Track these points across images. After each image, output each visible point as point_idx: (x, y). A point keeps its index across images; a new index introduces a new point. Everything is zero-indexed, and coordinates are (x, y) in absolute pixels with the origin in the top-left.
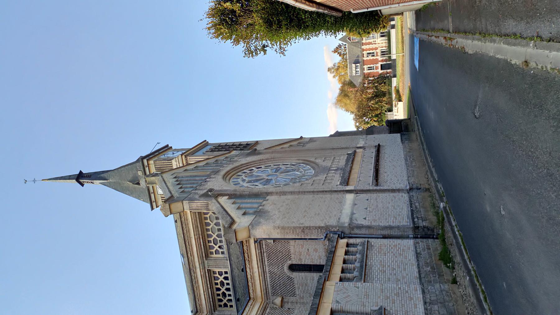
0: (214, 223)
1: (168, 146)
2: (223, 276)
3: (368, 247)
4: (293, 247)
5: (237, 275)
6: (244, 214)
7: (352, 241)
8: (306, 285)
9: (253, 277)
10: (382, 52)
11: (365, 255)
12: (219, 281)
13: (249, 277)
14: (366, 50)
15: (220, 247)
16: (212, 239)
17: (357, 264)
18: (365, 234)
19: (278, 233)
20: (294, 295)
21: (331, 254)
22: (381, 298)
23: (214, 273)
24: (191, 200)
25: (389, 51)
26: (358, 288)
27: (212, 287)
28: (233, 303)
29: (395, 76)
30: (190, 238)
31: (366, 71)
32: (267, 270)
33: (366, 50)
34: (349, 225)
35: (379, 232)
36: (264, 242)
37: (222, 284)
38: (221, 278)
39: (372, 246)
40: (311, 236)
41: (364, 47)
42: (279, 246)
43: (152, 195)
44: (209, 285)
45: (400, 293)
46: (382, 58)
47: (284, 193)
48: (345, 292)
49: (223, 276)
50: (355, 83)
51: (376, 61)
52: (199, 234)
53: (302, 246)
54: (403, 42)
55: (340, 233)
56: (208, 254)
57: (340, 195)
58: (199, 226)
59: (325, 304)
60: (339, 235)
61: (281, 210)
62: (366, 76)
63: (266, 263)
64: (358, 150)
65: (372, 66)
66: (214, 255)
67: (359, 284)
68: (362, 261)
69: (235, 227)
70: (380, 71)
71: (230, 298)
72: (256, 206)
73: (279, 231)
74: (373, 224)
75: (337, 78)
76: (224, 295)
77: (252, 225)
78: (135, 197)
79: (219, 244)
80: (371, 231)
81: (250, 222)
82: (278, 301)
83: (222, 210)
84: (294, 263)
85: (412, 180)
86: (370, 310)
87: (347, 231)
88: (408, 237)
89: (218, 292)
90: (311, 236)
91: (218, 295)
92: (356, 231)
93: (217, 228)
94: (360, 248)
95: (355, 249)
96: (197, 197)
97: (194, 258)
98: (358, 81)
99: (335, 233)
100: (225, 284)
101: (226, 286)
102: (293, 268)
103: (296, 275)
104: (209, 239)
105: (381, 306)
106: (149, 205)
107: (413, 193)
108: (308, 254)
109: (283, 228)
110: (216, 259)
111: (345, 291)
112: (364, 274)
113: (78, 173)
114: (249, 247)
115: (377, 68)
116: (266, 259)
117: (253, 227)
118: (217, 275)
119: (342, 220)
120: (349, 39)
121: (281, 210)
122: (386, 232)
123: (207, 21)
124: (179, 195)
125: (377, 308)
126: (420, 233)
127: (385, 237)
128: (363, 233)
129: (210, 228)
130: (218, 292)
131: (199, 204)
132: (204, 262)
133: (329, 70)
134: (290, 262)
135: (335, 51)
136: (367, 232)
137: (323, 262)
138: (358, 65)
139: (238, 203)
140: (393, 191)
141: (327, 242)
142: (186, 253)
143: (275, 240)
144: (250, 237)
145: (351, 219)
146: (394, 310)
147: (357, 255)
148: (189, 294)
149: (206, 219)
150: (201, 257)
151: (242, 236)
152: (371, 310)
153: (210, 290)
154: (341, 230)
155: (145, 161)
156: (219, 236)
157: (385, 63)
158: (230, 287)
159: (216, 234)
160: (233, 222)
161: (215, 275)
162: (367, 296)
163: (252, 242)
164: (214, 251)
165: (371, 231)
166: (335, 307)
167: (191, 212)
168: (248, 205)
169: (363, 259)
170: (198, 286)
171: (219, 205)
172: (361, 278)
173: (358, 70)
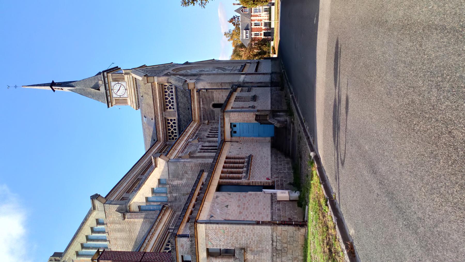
1: (117, 67)
10: (265, 23)
15: (172, 105)
16: (168, 100)
23: (168, 120)
25: (270, 24)
27: (166, 128)
29: (272, 41)
31: (253, 36)
33: (254, 20)
41: (252, 18)
43: (109, 98)
46: (265, 28)
47: (210, 74)
50: (245, 45)
51: (261, 30)
54: (278, 13)
57: (238, 76)
62: (253, 40)
64: (247, 64)
65: (258, 32)
66: (169, 110)
70: (263, 37)
73: (209, 85)
75: (232, 42)
76: (172, 132)
78: (96, 99)
79: (172, 103)
85: (273, 71)
87: (242, 84)
88: (268, 86)
91: (169, 133)
98: (247, 44)
99: (236, 85)
106: (106, 104)
107: (273, 75)
109: (212, 83)
113: (51, 82)
115: (261, 35)
118: (169, 121)
120: (242, 11)
122: (259, 85)
126: (273, 84)
133: (225, 34)
134: (213, 103)
135: (231, 21)
140: (264, 74)
143: (207, 89)
149: (165, 89)
155: (105, 73)
156: (172, 98)
157: (266, 31)
164: (168, 107)
173: (248, 35)
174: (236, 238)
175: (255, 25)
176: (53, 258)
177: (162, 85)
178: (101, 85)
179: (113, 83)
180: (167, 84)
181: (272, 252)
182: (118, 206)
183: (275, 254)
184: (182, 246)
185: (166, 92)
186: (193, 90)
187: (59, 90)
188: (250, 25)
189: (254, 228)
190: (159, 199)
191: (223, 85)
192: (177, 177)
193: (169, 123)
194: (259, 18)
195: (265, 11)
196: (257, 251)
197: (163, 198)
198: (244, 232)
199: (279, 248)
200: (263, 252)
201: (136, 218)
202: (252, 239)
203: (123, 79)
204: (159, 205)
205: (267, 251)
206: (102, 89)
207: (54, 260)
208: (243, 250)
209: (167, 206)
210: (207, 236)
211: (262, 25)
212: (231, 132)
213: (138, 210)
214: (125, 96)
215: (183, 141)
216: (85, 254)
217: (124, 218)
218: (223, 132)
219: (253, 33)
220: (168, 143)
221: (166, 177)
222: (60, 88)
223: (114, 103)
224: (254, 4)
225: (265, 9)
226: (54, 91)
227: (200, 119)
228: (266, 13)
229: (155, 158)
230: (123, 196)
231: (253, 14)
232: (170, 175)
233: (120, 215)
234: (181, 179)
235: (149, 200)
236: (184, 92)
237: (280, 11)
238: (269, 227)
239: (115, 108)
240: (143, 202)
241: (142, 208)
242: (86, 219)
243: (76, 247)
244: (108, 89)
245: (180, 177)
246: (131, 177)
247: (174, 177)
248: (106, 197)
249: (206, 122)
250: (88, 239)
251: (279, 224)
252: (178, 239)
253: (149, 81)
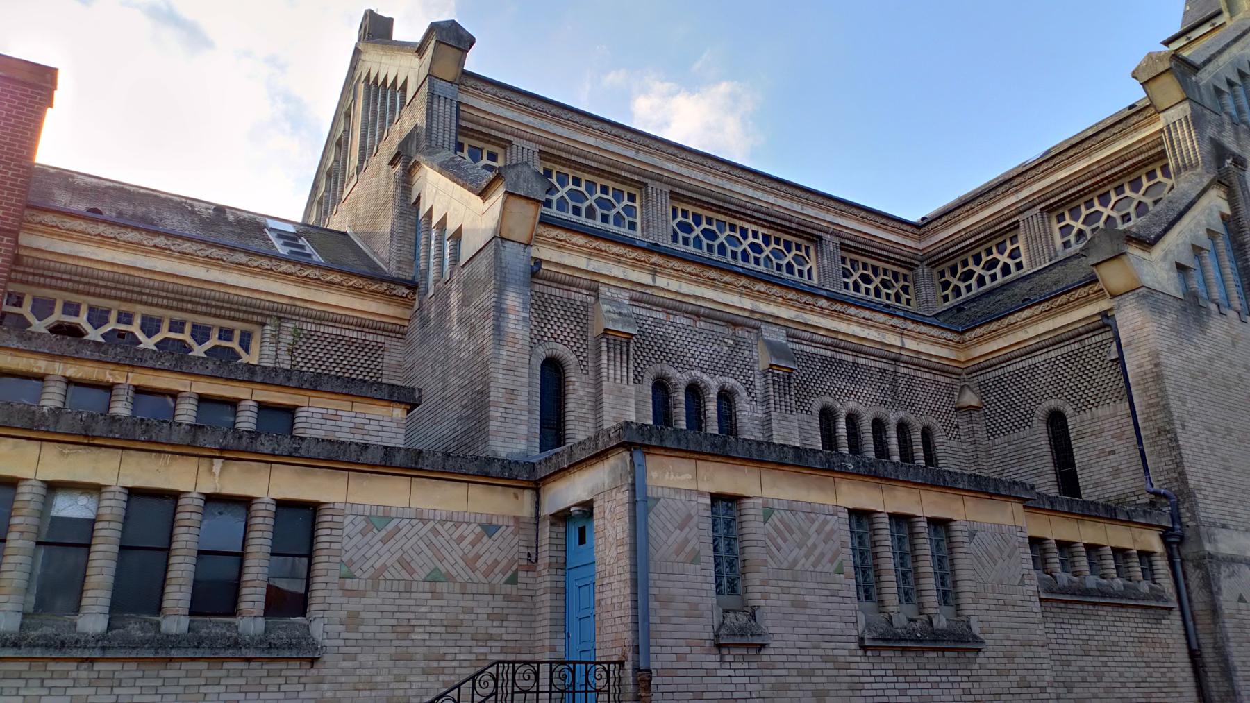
0: (1144, 199)
2: (1009, 261)
3: (1153, 609)
4: (1111, 414)
5: (1017, 291)
6: (1181, 268)
7: (1161, 565)
8: (1021, 460)
9: (1012, 328)
11: (1123, 602)
12: (995, 255)
13: (1011, 319)
16: (1097, 207)
17: (1091, 581)
18: (1190, 600)
19: (1140, 366)
20: (991, 433)
21: (1109, 513)
22: (1006, 643)
23: (1014, 239)
24: (1196, 121)
26: (1022, 584)
27: (979, 243)
28: (952, 301)
30: (1089, 155)
32: (1038, 359)
34: (1211, 556)
35: (1206, 640)
36: (1110, 335)
37: (992, 264)
38: (1004, 259)
39: (1158, 621)
40: (1152, 453)
42: (1109, 378)
43: (1206, 28)
44: (982, 235)
45: (1031, 690)
48: (1002, 552)
49: (1009, 261)
52: (1103, 172)
53: (1118, 437)
55: (1178, 532)
56: (1055, 209)
58: (1125, 165)
59: (960, 503)
60: (1173, 529)
61: (1217, 363)
63: (1053, 354)
66: (1056, 227)
67: (1032, 586)
68: (1103, 594)
69: (1134, 251)
71: (963, 290)
72: (1217, 293)
74: (1229, 624)
77: (1148, 296)
80: (1204, 619)
81: (1157, 287)
82: (970, 399)
83: (1181, 207)
86: (967, 613)
87: (1189, 550)
89: (970, 261)
90: (1152, 453)
92: (1194, 577)
93: (1132, 210)
94: (1145, 587)
95: (1139, 575)
96: (1210, 132)
97: (1039, 180)
99: (1176, 517)
100: (992, 272)
101: (987, 275)
102: (1056, 420)
103: (1038, 435)
104: (1096, 202)
105: (983, 642)
106: (1177, 29)
108: (1102, 454)
109: (1159, 377)
110: (1048, 234)
111: (1007, 551)
112: (1062, 598)
114: (1087, 300)
116: (1065, 350)
117: (1145, 297)
118: (1010, 247)
119: (1220, 534)
121: (1217, 363)
122: (1209, 656)
124: (1207, 86)
125: (976, 630)
127: (1195, 656)
128: (1193, 596)
129: (1128, 192)
130: (970, 261)
131: (1187, 144)
132: (1034, 206)
134: (1069, 411)
136: (1198, 607)
137: (1087, 494)
139: (1215, 245)
141: (1144, 499)
142: (1052, 159)
143: (1120, 361)
144: (1113, 296)
145: (1231, 560)
146: (981, 673)
147: (1118, 580)
148: (960, 199)
149: (1152, 175)
150: (1044, 195)
151: (1113, 276)
152: (968, 617)
153: (973, 240)
154: (1188, 533)
158: (989, 284)
159: (1113, 214)
160: (1147, 243)
161: (1008, 243)
162: (1005, 606)
163: (1103, 305)
164: (1068, 221)
165: (1204, 619)
166: (957, 528)
167: (1161, 131)
168: (1213, 273)
169: (1111, 596)
170: (976, 212)
171: (1194, 195)
172: (1053, 593)
177: (1162, 155)
186: (1100, 294)
191: (1163, 441)
193: (1001, 249)
215: (748, 303)
220: (923, 270)
230: (516, 141)
246: (642, 157)
253: (1153, 86)
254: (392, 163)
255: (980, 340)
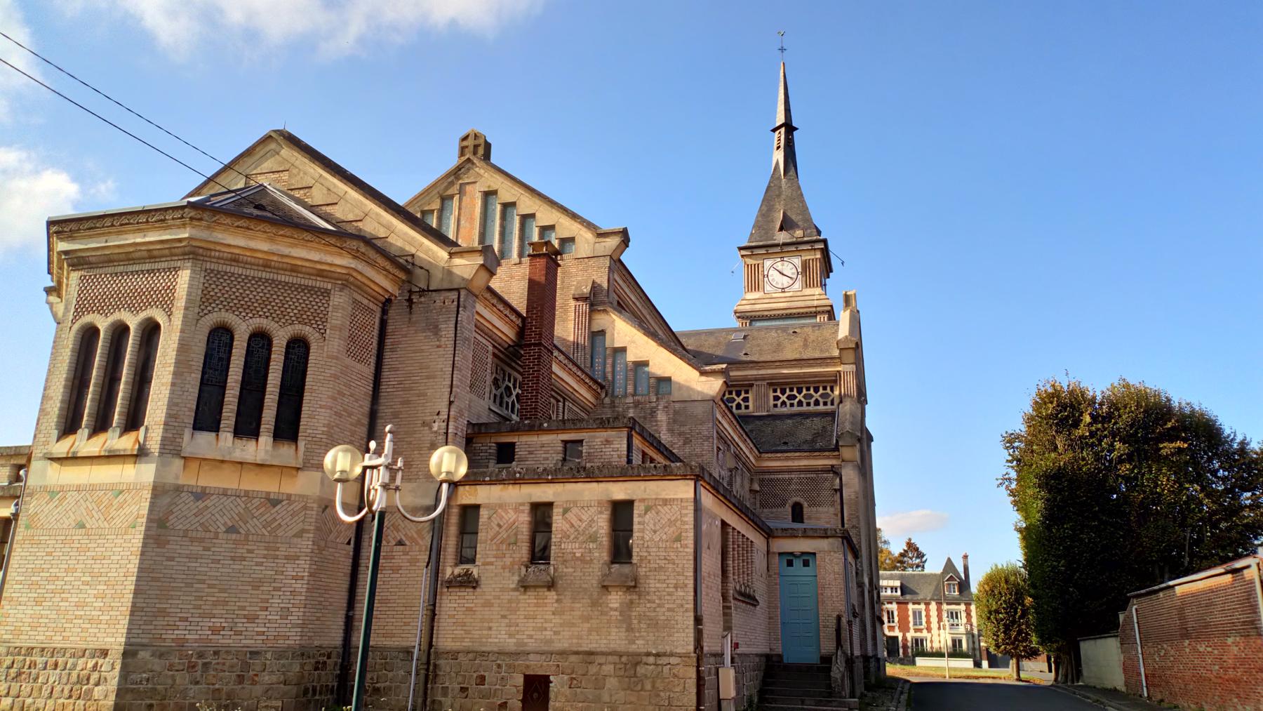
14: (928, 610)
15: (784, 403)
23: (747, 392)
33: (928, 610)
41: (933, 606)
46: (909, 639)
51: (904, 628)
54: (968, 677)
65: (896, 619)
66: (772, 394)
73: (853, 497)
78: (757, 221)
79: (788, 402)
84: (805, 510)
106: (745, 244)
118: (743, 395)
120: (951, 578)
123: (1064, 383)
134: (805, 505)
135: (911, 546)
138: (899, 593)
143: (841, 490)
150: (773, 377)
156: (800, 403)
163: (834, 462)
164: (778, 393)
174: (661, 568)
175: (914, 613)
176: (481, 141)
177: (835, 381)
178: (787, 229)
179: (797, 261)
180: (837, 393)
181: (628, 654)
182: (605, 285)
183: (624, 659)
184: (608, 442)
185: (816, 390)
186: (837, 457)
187: (776, 142)
188: (915, 598)
189: (687, 611)
190: (620, 378)
192: (675, 421)
194: (934, 625)
195: (954, 641)
196: (630, 617)
197: (621, 385)
198: (676, 587)
199: (641, 670)
200: (627, 631)
201: (577, 325)
202: (659, 606)
203: (807, 285)
204: (605, 377)
205: (632, 642)
206: (782, 237)
207: (477, 142)
208: (633, 586)
209: (603, 395)
210: (666, 502)
211: (916, 630)
212: (792, 554)
213: (595, 328)
214: (768, 288)
216: (490, 211)
217: (576, 299)
218: (792, 535)
219: (894, 607)
221: (676, 396)
222: (782, 144)
223: (750, 261)
224: (990, 612)
225: (960, 641)
226: (774, 130)
227: (764, 472)
228: (950, 643)
229: (722, 372)
231: (945, 607)
232: (683, 405)
233: (586, 290)
234: (671, 431)
235: (619, 355)
236: (823, 433)
237: (981, 681)
238: (691, 648)
239: (739, 264)
240: (613, 340)
241: (598, 339)
242: (574, 216)
243: (508, 193)
244: (783, 249)
245: (676, 427)
247: (676, 413)
248: (620, 261)
249: (756, 487)
250: (526, 218)
251: (698, 672)
252: (624, 434)
253: (845, 352)
254: (741, 316)
255: (770, 459)
